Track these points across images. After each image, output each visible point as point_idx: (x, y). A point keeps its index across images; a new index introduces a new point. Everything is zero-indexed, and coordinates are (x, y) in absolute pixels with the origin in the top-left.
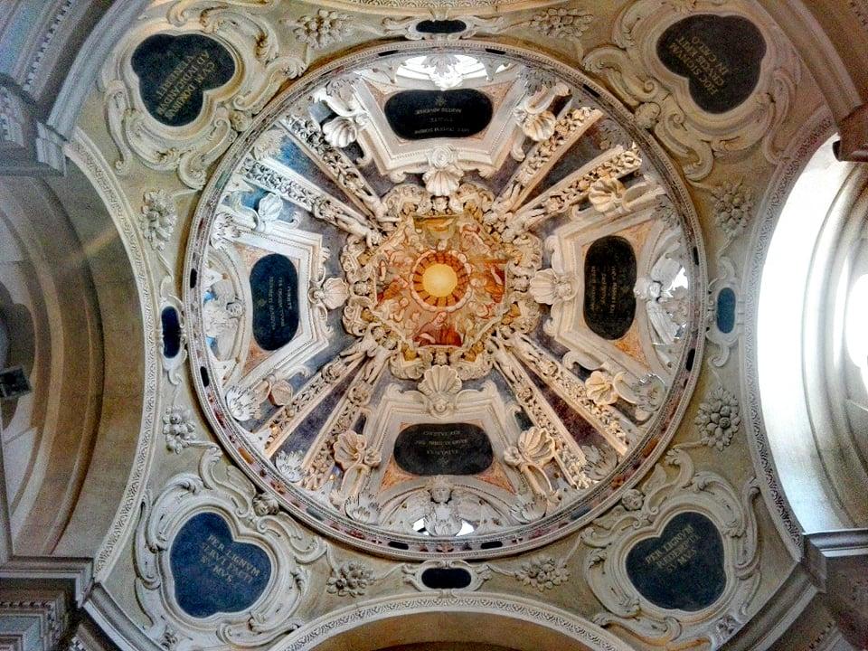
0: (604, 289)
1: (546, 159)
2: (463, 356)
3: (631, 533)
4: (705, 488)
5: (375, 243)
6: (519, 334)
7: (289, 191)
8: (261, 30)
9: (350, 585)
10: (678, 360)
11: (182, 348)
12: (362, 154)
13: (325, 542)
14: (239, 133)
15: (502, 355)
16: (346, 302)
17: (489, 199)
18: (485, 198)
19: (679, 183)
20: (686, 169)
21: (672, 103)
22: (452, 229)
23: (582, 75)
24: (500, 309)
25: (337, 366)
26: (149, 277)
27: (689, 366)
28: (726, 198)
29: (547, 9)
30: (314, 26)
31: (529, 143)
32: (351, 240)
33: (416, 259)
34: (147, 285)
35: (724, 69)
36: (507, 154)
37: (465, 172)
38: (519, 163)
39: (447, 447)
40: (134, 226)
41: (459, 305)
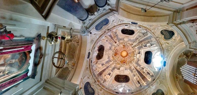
2: (113, 56)
3: (92, 83)
6: (115, 65)
7: (142, 37)
9: (92, 42)
10: (117, 91)
15: (113, 62)
19: (142, 91)
24: (119, 62)
25: (116, 38)
27: (116, 93)
29: (166, 77)
30: (168, 50)
31: (143, 69)
32: (133, 43)
33: (128, 51)
39: (100, 53)
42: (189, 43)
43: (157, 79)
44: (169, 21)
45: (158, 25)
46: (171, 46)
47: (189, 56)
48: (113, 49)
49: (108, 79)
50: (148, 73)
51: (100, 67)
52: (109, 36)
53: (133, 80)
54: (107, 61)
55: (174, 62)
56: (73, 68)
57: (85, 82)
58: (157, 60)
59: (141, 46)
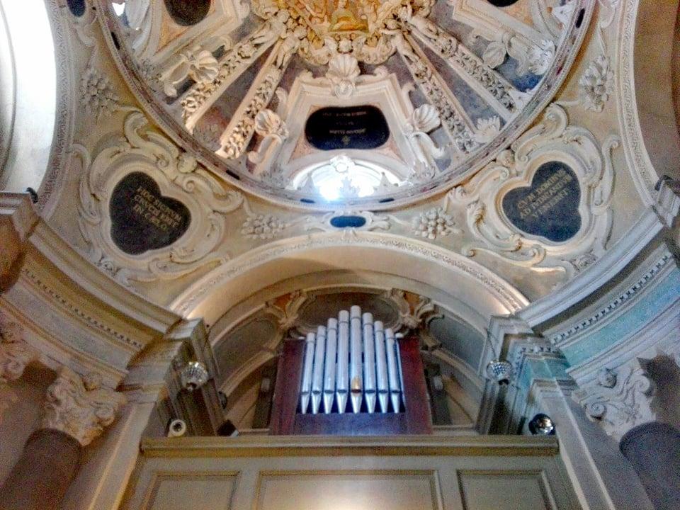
1: (258, 92)
5: (405, 8)
7: (476, 67)
8: (479, 229)
12: (410, 93)
17: (302, 49)
18: (306, 50)
20: (145, 121)
21: (172, 176)
22: (334, 17)
23: (242, 188)
26: (620, 35)
28: (106, 103)
29: (274, 239)
30: (440, 228)
31: (272, 106)
32: (425, 12)
34: (625, 26)
35: (138, 209)
36: (290, 93)
37: (324, 76)
38: (280, 85)
40: (619, 86)
42: (538, 332)
43: (242, 192)
46: (466, 237)
53: (188, 46)
58: (343, 177)
59: (408, 74)
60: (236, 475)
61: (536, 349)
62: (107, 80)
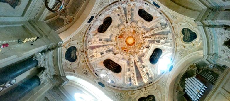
0: (113, 65)
2: (116, 37)
3: (79, 50)
4: (78, 64)
6: (114, 47)
7: (159, 29)
9: (101, 4)
11: (153, 5)
12: (157, 42)
13: (110, 4)
14: (175, 35)
15: (113, 43)
16: (137, 25)
24: (120, 47)
25: (130, 17)
29: (166, 83)
30: (182, 54)
31: (144, 67)
32: (146, 32)
38: (141, 63)
39: (105, 26)
41: (125, 41)
42: (209, 54)
44: (197, 19)
45: (183, 19)
46: (186, 51)
47: (201, 70)
48: (121, 29)
49: (97, 57)
50: (147, 73)
51: (96, 41)
52: (124, 8)
54: (108, 39)
55: (181, 71)
56: (68, 24)
57: (72, 46)
59: (153, 40)
60: (206, 60)
61: (212, 57)
62: (119, 93)
